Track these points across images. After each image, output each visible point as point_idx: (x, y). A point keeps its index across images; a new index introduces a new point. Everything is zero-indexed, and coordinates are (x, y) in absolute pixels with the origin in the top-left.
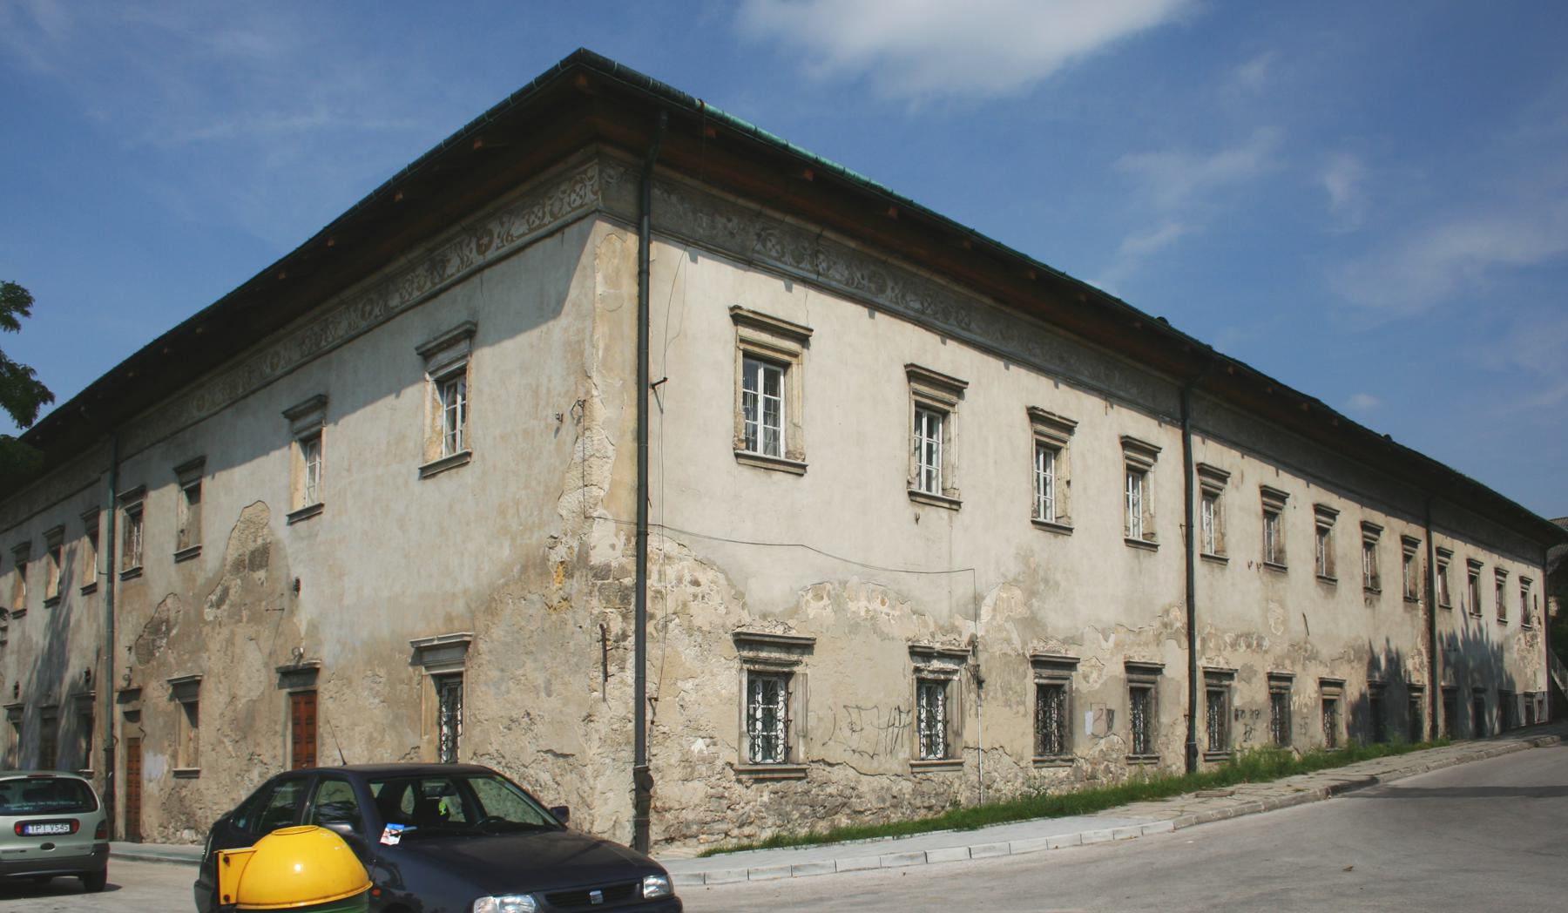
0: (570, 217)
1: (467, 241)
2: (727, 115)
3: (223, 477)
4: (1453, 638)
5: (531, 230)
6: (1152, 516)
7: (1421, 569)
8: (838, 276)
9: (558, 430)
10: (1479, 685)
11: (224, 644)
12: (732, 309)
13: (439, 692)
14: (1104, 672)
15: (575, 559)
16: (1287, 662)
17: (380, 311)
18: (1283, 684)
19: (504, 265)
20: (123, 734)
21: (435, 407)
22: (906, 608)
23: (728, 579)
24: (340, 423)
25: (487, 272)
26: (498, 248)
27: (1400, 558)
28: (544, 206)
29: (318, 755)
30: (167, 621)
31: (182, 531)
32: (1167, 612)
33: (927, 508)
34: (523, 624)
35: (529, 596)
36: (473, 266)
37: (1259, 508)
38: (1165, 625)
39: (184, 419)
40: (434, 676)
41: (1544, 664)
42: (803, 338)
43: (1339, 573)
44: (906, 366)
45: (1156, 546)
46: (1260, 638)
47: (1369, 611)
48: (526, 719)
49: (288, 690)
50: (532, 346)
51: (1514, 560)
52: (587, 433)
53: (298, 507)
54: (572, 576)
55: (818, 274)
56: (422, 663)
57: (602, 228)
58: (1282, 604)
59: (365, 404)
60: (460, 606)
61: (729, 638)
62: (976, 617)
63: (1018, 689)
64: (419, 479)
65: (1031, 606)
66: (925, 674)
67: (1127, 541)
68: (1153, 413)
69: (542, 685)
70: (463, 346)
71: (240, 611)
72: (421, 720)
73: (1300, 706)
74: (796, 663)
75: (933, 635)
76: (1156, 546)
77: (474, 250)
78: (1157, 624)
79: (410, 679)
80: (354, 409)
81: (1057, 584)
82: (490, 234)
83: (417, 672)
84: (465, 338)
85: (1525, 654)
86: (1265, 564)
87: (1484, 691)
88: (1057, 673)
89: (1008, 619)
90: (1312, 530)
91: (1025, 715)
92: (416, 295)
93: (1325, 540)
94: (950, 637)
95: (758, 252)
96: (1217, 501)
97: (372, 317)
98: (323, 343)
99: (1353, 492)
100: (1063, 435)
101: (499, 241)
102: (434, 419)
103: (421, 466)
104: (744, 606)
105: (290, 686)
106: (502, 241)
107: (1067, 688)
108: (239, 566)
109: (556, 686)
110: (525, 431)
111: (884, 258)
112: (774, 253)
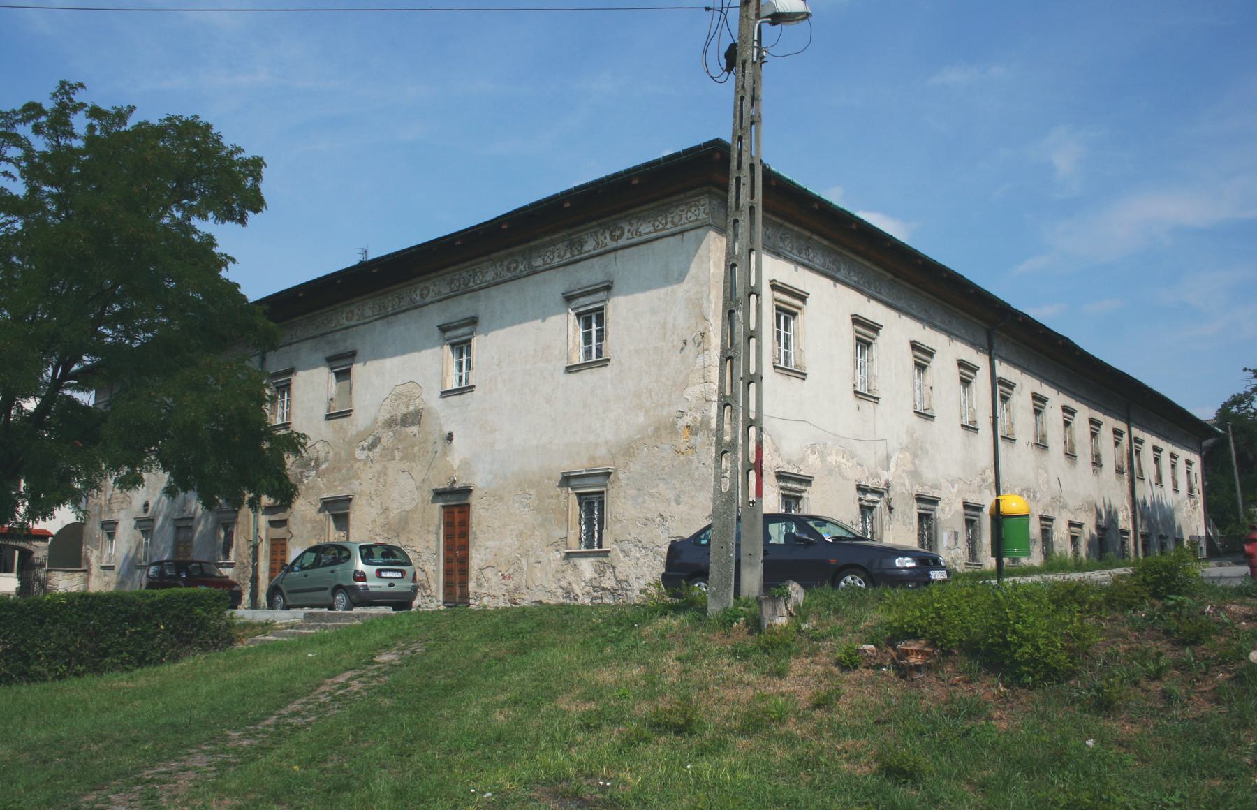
0: (688, 226)
1: (601, 231)
2: (780, 173)
3: (374, 365)
4: (1144, 503)
5: (656, 231)
6: (975, 411)
7: (1125, 452)
8: (818, 262)
9: (682, 349)
10: (1163, 533)
11: (376, 475)
12: (771, 281)
13: (580, 505)
14: (952, 508)
15: (698, 425)
16: (1050, 509)
17: (525, 267)
18: (1049, 523)
19: (633, 249)
20: (267, 536)
21: (575, 330)
22: (855, 461)
23: (772, 440)
24: (490, 335)
25: (620, 252)
26: (628, 239)
27: (1113, 444)
28: (666, 217)
29: (471, 544)
30: (317, 459)
31: (332, 399)
32: (984, 472)
33: (864, 401)
34: (656, 462)
35: (661, 446)
36: (607, 248)
37: (1031, 407)
38: (983, 480)
39: (333, 325)
40: (577, 494)
41: (1203, 521)
42: (803, 298)
43: (1078, 452)
44: (852, 316)
45: (977, 429)
46: (1035, 492)
47: (1095, 478)
48: (659, 519)
49: (442, 504)
50: (660, 299)
51: (1182, 449)
52: (706, 352)
53: (449, 388)
54: (696, 434)
55: (809, 260)
56: (568, 485)
57: (712, 234)
58: (1046, 471)
59: (513, 324)
60: (602, 451)
61: (773, 474)
62: (888, 469)
63: (909, 515)
64: (565, 373)
65: (914, 464)
66: (863, 502)
67: (962, 426)
68: (973, 345)
69: (673, 498)
70: (602, 295)
71: (392, 452)
72: (568, 521)
73: (1058, 540)
74: (804, 491)
75: (867, 479)
76: (977, 429)
78: (979, 479)
79: (558, 496)
80: (502, 327)
81: (927, 450)
82: (622, 230)
83: (564, 492)
84: (603, 290)
85: (1190, 514)
86: (1036, 444)
87: (1166, 537)
88: (929, 506)
89: (904, 471)
90: (1062, 423)
91: (913, 532)
92: (557, 260)
93: (1068, 429)
94: (876, 480)
95: (782, 248)
96: (1008, 402)
97: (518, 271)
98: (471, 284)
99: (1084, 398)
100: (928, 358)
102: (575, 337)
104: (779, 456)
105: (443, 502)
106: (632, 234)
107: (933, 516)
108: (390, 423)
109: (684, 498)
110: (655, 348)
111: (840, 250)
112: (788, 249)
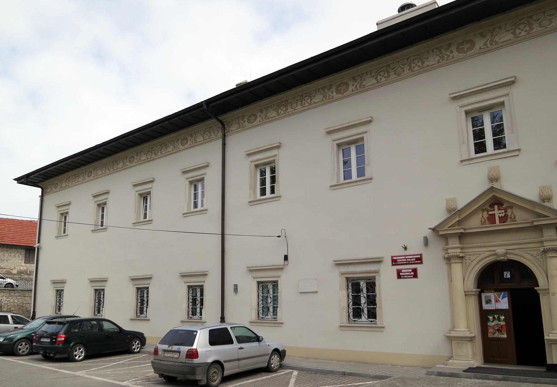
77: (87, 176)
101: (94, 175)
103: (330, 185)
